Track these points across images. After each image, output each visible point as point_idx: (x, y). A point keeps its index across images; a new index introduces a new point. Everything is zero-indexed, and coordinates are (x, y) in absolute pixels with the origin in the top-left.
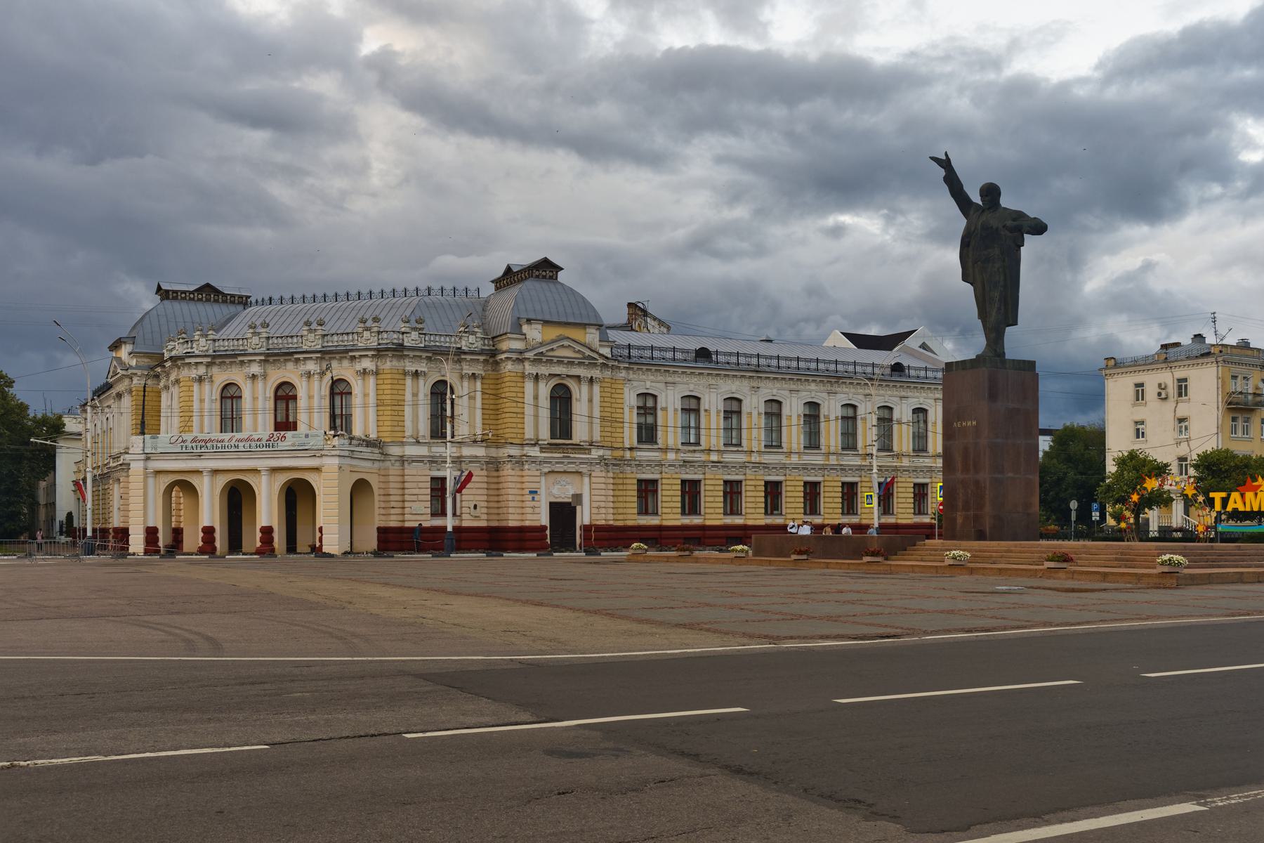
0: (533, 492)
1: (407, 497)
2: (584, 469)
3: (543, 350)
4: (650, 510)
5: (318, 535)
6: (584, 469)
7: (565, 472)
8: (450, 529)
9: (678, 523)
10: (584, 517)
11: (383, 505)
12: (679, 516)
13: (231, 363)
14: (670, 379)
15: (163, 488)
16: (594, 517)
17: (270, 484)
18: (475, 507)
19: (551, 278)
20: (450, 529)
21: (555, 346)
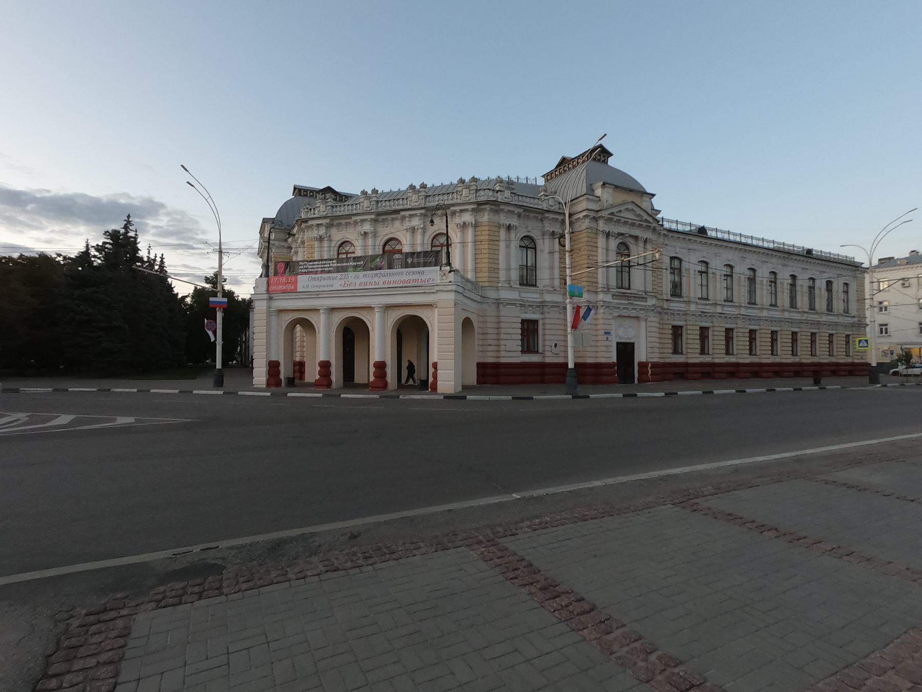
0: (607, 333)
1: (502, 336)
2: (642, 314)
3: (614, 210)
4: (532, 349)
5: (431, 370)
6: (642, 314)
7: (629, 317)
8: (571, 365)
9: (697, 361)
10: (641, 355)
11: (481, 342)
12: (698, 355)
13: (347, 224)
14: (690, 247)
15: (284, 325)
16: (650, 355)
17: (383, 320)
18: (556, 345)
19: (604, 161)
20: (571, 365)
21: (622, 208)
